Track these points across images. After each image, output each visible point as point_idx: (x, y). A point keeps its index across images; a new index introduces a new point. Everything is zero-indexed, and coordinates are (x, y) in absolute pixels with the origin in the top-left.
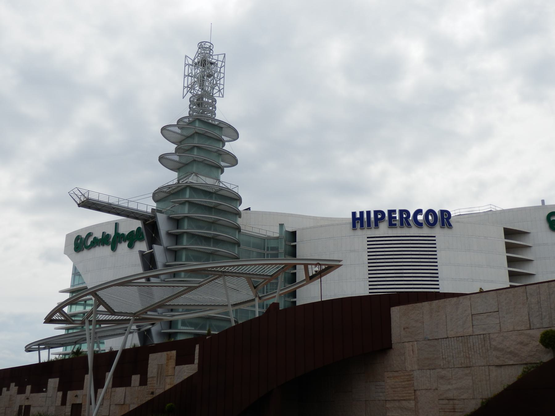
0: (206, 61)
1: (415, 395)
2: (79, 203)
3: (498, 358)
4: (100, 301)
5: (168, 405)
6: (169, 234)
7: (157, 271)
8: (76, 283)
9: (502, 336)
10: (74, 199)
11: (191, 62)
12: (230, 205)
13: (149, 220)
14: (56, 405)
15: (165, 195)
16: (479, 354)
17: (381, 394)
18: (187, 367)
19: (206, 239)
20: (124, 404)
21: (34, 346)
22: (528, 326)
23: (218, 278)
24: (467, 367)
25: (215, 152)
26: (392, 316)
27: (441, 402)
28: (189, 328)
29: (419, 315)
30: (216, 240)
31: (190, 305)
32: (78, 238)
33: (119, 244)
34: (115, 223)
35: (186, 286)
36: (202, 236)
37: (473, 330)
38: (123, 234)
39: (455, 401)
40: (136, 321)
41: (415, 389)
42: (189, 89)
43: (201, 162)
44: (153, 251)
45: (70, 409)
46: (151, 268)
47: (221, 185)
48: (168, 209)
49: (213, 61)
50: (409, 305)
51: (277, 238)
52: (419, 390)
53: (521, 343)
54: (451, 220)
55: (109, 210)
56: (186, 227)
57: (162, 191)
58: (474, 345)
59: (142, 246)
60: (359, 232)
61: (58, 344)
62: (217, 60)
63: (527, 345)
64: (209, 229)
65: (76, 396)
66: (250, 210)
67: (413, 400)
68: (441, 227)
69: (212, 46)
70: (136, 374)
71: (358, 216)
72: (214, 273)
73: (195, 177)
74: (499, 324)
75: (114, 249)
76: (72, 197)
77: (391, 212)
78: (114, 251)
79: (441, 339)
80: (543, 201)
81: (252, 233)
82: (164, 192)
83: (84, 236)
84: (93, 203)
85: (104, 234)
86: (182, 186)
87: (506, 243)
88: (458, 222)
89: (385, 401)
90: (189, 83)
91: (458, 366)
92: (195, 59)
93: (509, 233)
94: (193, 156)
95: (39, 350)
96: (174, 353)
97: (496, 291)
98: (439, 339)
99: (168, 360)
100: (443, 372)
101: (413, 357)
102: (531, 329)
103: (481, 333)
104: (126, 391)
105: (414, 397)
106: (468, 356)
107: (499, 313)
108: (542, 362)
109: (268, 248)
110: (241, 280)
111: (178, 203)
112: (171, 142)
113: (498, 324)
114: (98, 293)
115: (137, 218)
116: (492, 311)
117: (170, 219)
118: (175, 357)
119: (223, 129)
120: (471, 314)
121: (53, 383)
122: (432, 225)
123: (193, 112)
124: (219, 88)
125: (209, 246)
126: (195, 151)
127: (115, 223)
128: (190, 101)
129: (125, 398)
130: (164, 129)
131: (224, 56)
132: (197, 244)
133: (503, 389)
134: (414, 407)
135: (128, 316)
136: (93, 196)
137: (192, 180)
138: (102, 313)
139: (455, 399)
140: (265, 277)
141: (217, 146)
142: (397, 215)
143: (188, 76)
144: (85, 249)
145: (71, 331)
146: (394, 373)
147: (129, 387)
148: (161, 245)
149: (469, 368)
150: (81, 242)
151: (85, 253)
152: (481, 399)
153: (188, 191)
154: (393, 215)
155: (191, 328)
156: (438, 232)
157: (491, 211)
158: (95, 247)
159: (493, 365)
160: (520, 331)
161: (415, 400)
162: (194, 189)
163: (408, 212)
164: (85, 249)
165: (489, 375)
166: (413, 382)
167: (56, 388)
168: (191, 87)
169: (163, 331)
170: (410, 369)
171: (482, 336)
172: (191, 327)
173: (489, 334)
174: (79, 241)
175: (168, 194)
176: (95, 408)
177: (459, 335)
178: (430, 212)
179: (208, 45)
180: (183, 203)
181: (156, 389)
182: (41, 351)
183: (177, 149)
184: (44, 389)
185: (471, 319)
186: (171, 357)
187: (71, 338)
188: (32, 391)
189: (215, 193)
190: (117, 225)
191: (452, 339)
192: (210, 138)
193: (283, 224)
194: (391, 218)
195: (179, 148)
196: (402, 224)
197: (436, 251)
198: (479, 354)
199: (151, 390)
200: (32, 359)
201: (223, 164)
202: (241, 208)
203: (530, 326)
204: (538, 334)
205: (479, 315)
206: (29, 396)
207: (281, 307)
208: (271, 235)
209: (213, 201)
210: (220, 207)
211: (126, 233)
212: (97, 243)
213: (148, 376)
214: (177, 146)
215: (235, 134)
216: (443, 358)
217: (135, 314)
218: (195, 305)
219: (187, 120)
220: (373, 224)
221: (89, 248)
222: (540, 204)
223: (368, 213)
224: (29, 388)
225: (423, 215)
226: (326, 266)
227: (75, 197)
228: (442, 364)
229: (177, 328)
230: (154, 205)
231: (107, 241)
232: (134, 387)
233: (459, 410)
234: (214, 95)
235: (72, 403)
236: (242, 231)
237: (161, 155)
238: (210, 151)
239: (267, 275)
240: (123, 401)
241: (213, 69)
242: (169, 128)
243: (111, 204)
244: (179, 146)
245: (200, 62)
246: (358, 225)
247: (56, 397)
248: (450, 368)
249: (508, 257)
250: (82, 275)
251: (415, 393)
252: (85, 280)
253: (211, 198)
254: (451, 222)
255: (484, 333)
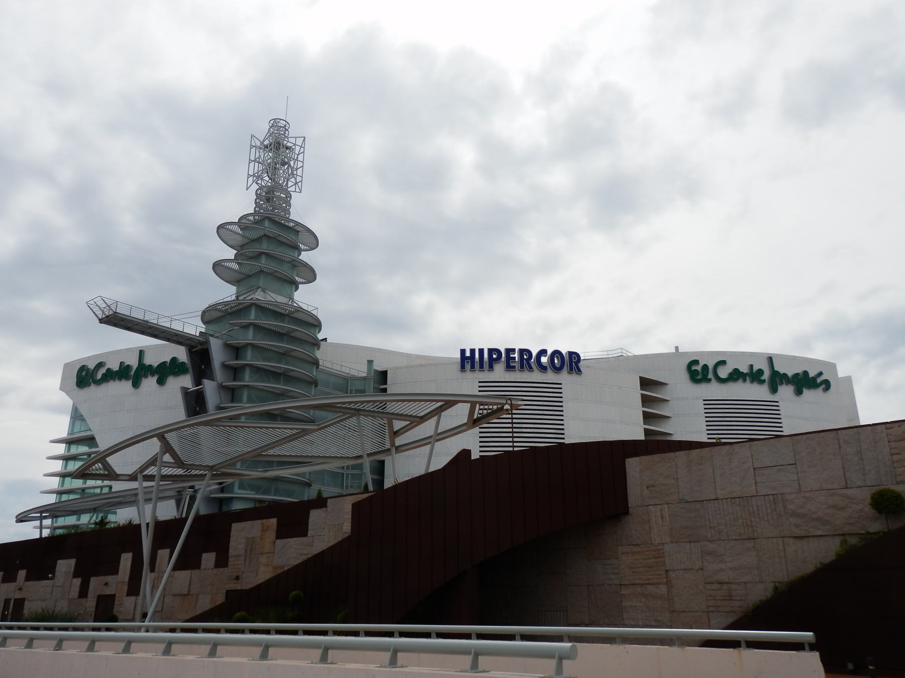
0: (280, 145)
1: (667, 577)
2: (101, 318)
3: (797, 526)
4: (167, 448)
5: (294, 593)
6: (225, 366)
7: (208, 415)
8: (77, 429)
9: (804, 497)
10: (94, 313)
11: (258, 144)
12: (307, 331)
13: (196, 347)
14: (70, 597)
15: (220, 314)
16: (768, 521)
17: (613, 577)
18: (295, 541)
19: (275, 375)
20: (188, 594)
21: (34, 513)
22: (844, 483)
23: (351, 417)
24: (748, 539)
25: (288, 262)
26: (627, 470)
27: (708, 586)
28: (249, 492)
29: (670, 469)
30: (286, 377)
31: (291, 456)
32: (83, 368)
33: (143, 379)
34: (140, 351)
35: (297, 429)
36: (270, 371)
37: (756, 489)
38: (150, 366)
39: (732, 585)
40: (214, 476)
41: (666, 569)
42: (255, 178)
43: (270, 274)
44: (202, 388)
45: (95, 603)
46: (199, 411)
47: (295, 305)
48: (224, 332)
49: (289, 144)
50: (654, 456)
51: (364, 378)
52: (674, 570)
53: (834, 507)
54: (581, 365)
55: (143, 330)
56: (249, 358)
57: (216, 309)
58: (758, 510)
59: (186, 381)
60: (469, 375)
61: (68, 511)
62: (295, 145)
63: (843, 509)
64: (279, 362)
65: (106, 584)
66: (326, 341)
67: (665, 584)
68: (569, 373)
69: (288, 125)
70: (208, 551)
71: (468, 354)
72: (344, 411)
73: (262, 293)
74: (797, 481)
75: (136, 385)
76: (91, 309)
77: (509, 351)
78: (137, 388)
79: (707, 500)
80: (677, 348)
81: (332, 371)
82: (218, 310)
83: (92, 366)
84: (121, 318)
85: (123, 365)
86: (245, 303)
87: (642, 395)
88: (588, 367)
89: (619, 586)
90: (256, 171)
91: (734, 537)
92: (264, 140)
93: (646, 383)
94: (260, 265)
95: (41, 518)
96: (274, 521)
97: (790, 437)
98: (703, 501)
99: (263, 531)
100: (711, 546)
101: (662, 526)
102: (848, 487)
103: (770, 493)
104: (191, 575)
105: (665, 580)
106: (750, 524)
107: (796, 467)
108: (868, 533)
109: (351, 391)
110: (340, 427)
111: (238, 326)
112: (228, 245)
113: (796, 480)
114: (166, 436)
115: (180, 343)
116: (784, 463)
117: (227, 346)
118: (275, 527)
119: (300, 233)
120: (752, 468)
121: (65, 566)
122: (557, 370)
123: (260, 209)
124: (296, 179)
125: (279, 383)
126: (263, 260)
127: (140, 351)
128: (256, 194)
129: (190, 585)
130: (223, 227)
131: (304, 140)
132: (264, 382)
133: (814, 569)
134: (666, 593)
135: (201, 470)
136: (123, 310)
137: (259, 296)
138: (167, 465)
139: (732, 583)
140: (413, 419)
141: (292, 255)
142: (516, 355)
143: (255, 161)
144: (92, 384)
145: (65, 497)
146: (633, 547)
147: (197, 570)
148: (213, 380)
149: (752, 540)
150: (86, 374)
151: (93, 390)
152: (772, 582)
153: (253, 312)
154: (512, 356)
155: (251, 492)
156: (564, 378)
157: (622, 356)
158: (108, 381)
159: (789, 537)
160: (831, 491)
161: (666, 584)
162: (261, 308)
163: (529, 352)
164: (92, 384)
165: (784, 550)
166: (663, 559)
167: (70, 572)
168: (258, 177)
169: (212, 496)
170: (657, 542)
171: (771, 498)
172: (251, 490)
173: (782, 494)
174: (84, 373)
175: (224, 314)
176: (152, 601)
177: (734, 495)
178: (556, 353)
179: (282, 123)
180: (246, 327)
181: (243, 572)
182: (43, 521)
183: (236, 255)
184: (50, 575)
185: (753, 474)
186: (268, 527)
187: (97, 502)
188: (28, 579)
189: (287, 315)
190: (141, 353)
191: (724, 501)
192: (282, 243)
193: (372, 361)
194: (509, 359)
195: (241, 254)
196: (522, 367)
197: (562, 402)
198: (768, 521)
199: (235, 574)
200: (29, 532)
201: (298, 279)
202: (320, 336)
203: (846, 483)
204: (865, 495)
205: (765, 468)
206: (23, 586)
207: (475, 455)
208: (354, 373)
209: (287, 326)
210: (295, 334)
211: (155, 365)
212: (110, 376)
213: (230, 555)
214: (236, 252)
215: (314, 241)
216: (710, 527)
217: (212, 467)
218: (302, 456)
219: (251, 218)
220: (486, 366)
221: (98, 383)
222: (674, 351)
223: (481, 351)
224: (22, 574)
225: (547, 357)
226: (499, 406)
227: (96, 309)
228: (709, 535)
229: (232, 492)
230: (202, 328)
231: (127, 374)
232: (205, 569)
233: (738, 598)
234: (289, 190)
235: (98, 593)
236: (320, 367)
237: (215, 262)
238: (280, 259)
239: (416, 417)
240: (187, 590)
241: (289, 155)
242: (229, 227)
243: (147, 322)
244: (240, 251)
245: (273, 144)
246: (468, 366)
247: (71, 586)
248: (722, 540)
249: (643, 412)
250: (86, 420)
251: (666, 574)
252: (91, 427)
253: (283, 321)
254: (580, 366)
255: (774, 492)
